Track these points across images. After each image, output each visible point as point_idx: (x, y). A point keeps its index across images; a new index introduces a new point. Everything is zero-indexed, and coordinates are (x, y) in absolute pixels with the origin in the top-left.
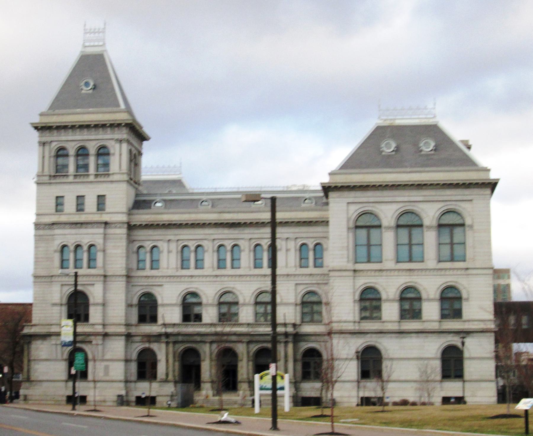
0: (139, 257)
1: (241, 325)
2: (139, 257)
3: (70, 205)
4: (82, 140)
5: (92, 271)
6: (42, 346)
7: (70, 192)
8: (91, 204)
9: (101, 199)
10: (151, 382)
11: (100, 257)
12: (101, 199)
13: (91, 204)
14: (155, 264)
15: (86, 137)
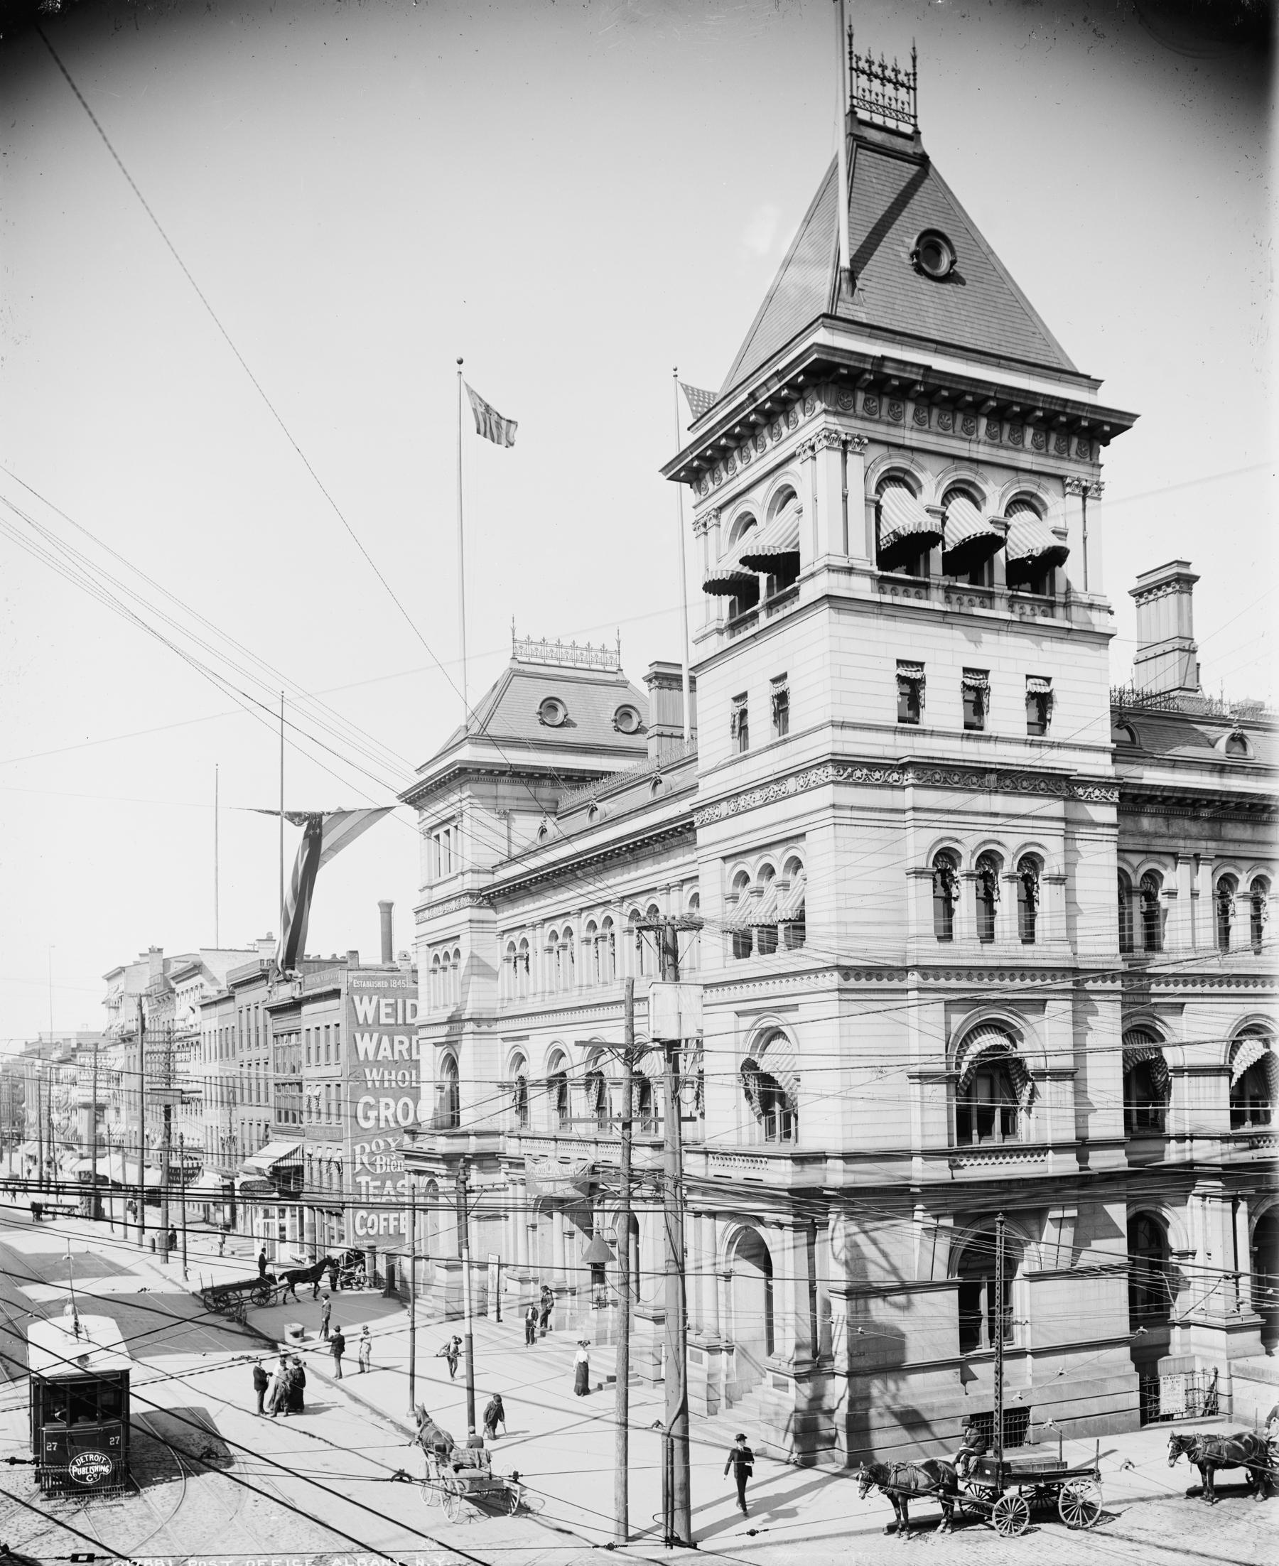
3: (943, 705)
8: (1007, 712)
13: (1007, 712)
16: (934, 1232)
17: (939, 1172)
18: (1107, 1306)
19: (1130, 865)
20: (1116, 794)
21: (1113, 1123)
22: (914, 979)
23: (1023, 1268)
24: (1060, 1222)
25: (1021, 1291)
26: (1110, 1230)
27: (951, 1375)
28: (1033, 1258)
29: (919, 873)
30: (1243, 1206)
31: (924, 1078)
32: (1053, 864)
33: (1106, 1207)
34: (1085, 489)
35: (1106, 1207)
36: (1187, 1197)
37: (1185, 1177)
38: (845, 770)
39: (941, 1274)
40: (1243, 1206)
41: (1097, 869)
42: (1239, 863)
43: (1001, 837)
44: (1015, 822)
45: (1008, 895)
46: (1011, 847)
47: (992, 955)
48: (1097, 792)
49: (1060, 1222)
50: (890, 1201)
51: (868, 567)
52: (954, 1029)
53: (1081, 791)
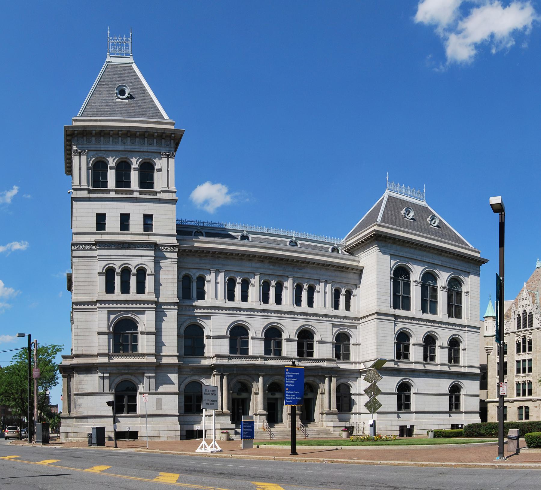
0: (190, 288)
1: (437, 365)
2: (190, 288)
3: (113, 224)
4: (124, 151)
5: (141, 297)
6: (85, 379)
7: (113, 212)
8: (136, 224)
9: (148, 218)
10: (179, 394)
11: (149, 282)
12: (148, 218)
13: (136, 224)
14: (201, 295)
15: (129, 147)
16: (103, 378)
17: (105, 360)
18: (172, 404)
20: (177, 249)
21: (79, 288)
24: (150, 377)
26: (171, 383)
28: (141, 388)
29: (99, 274)
30: (225, 378)
31: (100, 333)
33: (169, 375)
34: (168, 155)
35: (169, 375)
36: (211, 375)
39: (107, 390)
40: (225, 378)
41: (169, 274)
42: (342, 284)
43: (130, 262)
44: (143, 258)
46: (133, 265)
48: (169, 248)
49: (150, 377)
53: (163, 248)
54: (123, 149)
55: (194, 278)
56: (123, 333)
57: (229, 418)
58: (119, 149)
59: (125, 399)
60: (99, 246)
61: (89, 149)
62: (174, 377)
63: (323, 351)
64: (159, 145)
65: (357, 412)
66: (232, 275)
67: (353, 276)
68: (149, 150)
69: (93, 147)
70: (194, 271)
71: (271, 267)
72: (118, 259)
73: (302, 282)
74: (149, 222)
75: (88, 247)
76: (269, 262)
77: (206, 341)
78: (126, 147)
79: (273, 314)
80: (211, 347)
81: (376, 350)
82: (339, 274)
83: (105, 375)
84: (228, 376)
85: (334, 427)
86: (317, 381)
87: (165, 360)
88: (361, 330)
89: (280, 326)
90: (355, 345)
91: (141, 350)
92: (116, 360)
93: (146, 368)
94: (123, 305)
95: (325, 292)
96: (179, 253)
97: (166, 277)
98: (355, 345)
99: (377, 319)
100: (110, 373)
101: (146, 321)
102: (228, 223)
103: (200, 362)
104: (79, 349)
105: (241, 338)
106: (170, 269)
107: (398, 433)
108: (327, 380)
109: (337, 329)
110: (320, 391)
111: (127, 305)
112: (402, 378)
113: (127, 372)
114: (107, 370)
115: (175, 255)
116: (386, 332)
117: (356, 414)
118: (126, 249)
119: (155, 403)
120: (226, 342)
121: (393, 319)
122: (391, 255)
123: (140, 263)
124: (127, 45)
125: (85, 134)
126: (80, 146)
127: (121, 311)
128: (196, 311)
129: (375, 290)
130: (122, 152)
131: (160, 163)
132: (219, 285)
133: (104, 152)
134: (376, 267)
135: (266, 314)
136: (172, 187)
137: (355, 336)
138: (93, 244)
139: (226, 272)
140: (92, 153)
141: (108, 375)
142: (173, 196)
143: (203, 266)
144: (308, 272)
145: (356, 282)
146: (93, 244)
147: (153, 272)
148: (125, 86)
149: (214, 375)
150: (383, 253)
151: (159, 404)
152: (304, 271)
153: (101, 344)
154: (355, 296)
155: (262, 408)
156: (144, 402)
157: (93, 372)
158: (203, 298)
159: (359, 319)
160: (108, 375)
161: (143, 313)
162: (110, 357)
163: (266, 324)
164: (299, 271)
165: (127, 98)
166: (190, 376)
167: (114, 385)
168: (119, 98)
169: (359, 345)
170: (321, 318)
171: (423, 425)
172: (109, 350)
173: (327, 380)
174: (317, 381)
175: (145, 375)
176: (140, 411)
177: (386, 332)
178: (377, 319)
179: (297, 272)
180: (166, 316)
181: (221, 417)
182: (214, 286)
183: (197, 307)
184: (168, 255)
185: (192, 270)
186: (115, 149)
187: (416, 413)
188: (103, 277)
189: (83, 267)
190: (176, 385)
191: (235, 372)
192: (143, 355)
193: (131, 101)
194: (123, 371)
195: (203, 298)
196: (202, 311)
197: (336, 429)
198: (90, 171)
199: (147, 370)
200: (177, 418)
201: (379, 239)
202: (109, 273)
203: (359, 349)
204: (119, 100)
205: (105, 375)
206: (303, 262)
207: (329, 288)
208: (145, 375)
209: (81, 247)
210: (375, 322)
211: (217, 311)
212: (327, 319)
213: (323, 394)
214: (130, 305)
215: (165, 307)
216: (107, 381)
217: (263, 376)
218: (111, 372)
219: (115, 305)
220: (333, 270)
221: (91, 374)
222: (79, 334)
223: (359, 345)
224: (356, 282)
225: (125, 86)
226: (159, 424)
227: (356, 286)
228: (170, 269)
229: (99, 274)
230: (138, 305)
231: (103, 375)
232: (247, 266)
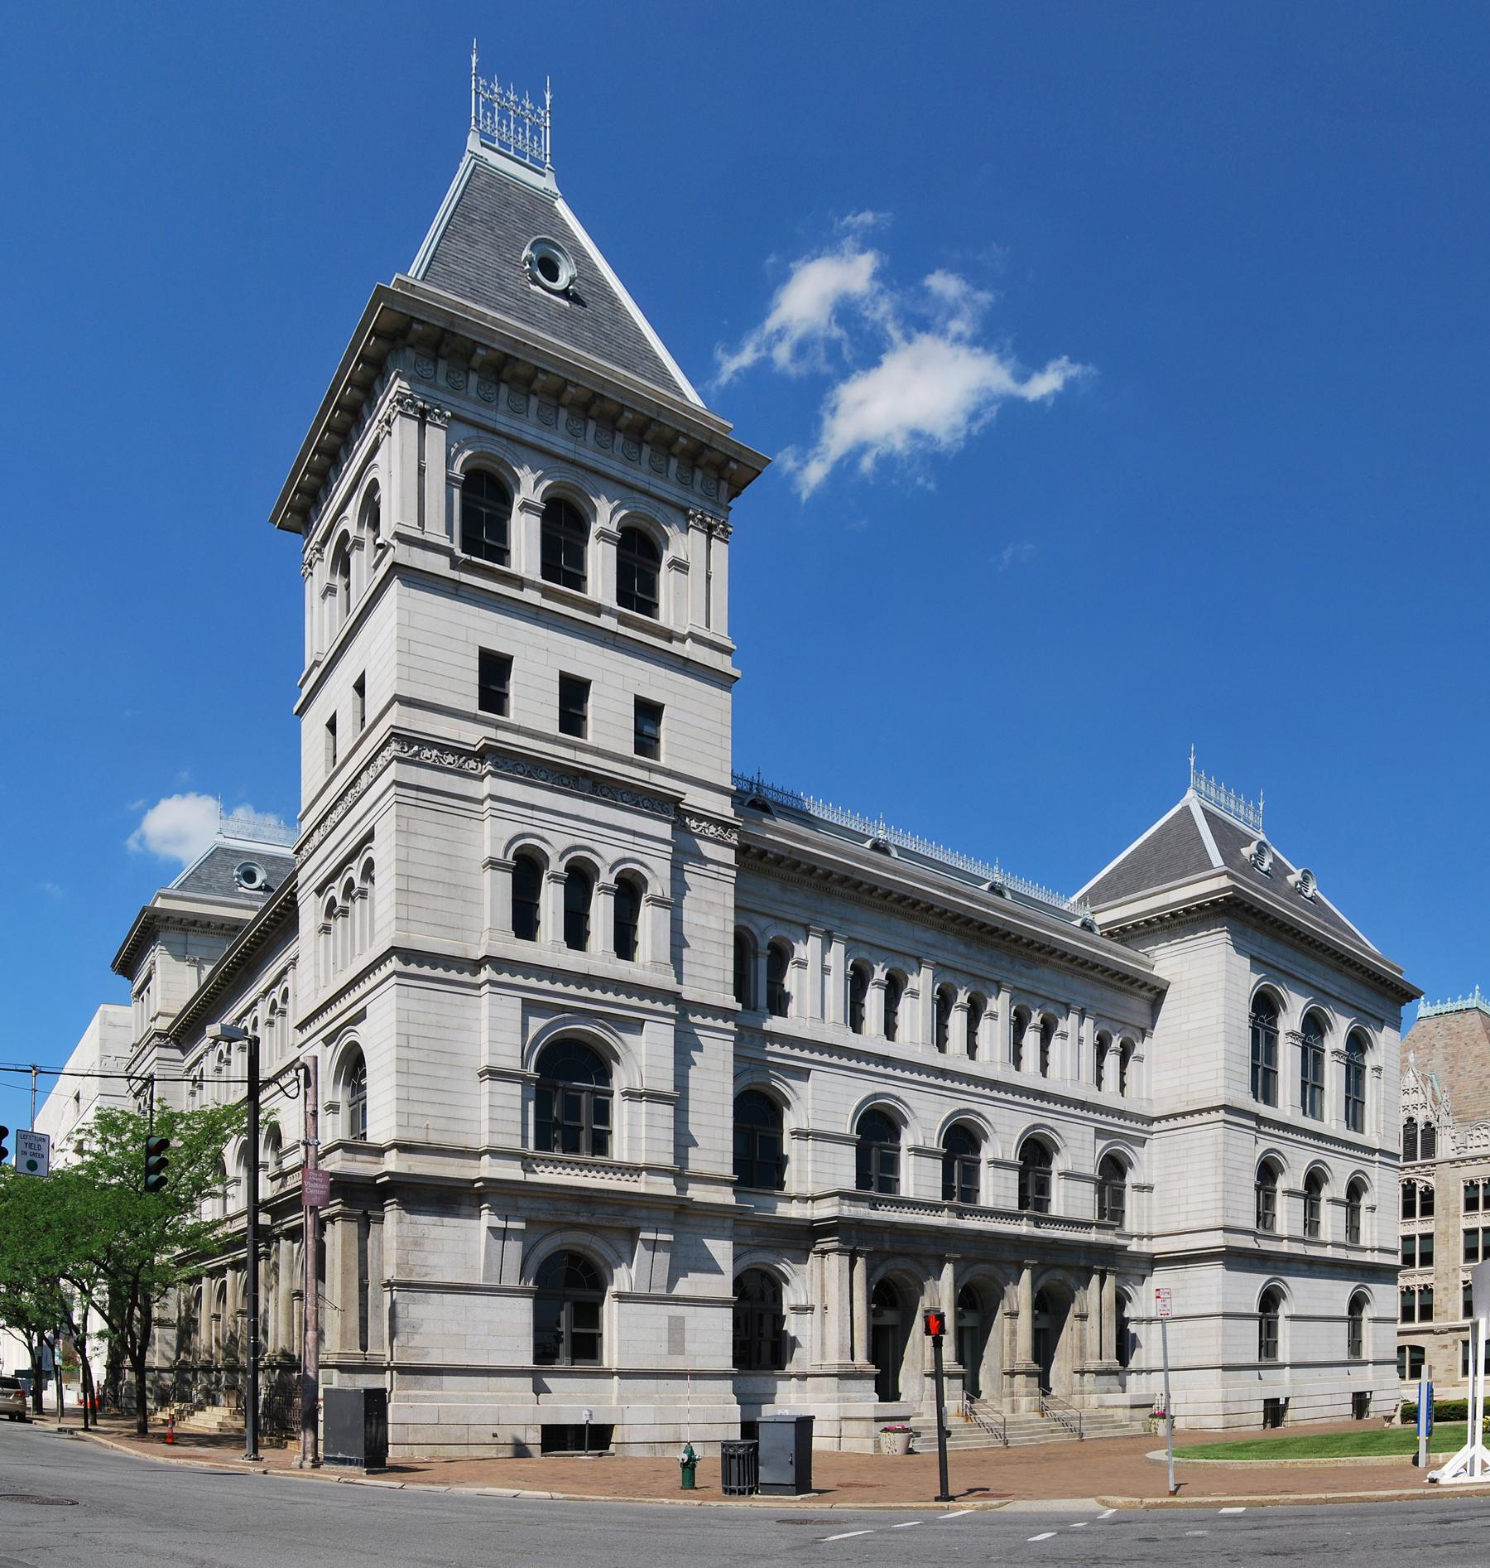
0: (760, 972)
2: (760, 972)
3: (532, 704)
4: (573, 463)
11: (650, 923)
16: (502, 1234)
17: (512, 1171)
18: (712, 1337)
19: (756, 926)
22: (486, 973)
23: (612, 1289)
25: (611, 1311)
26: (709, 1266)
27: (528, 1382)
28: (623, 1279)
29: (493, 864)
31: (494, 1074)
32: (659, 884)
33: (707, 1242)
34: (711, 528)
35: (707, 1242)
36: (808, 1251)
37: (803, 1238)
38: (410, 748)
39: (511, 1280)
41: (712, 909)
45: (601, 911)
46: (608, 857)
47: (572, 960)
48: (712, 829)
49: (654, 1246)
50: (444, 1198)
51: (445, 542)
52: (532, 1033)
53: (694, 824)
54: (571, 456)
55: (763, 945)
56: (567, 1083)
57: (871, 1384)
58: (558, 450)
59: (563, 1314)
60: (496, 766)
61: (456, 411)
62: (721, 1250)
63: (1071, 1199)
64: (684, 482)
65: (1144, 1366)
66: (864, 955)
67: (1137, 1006)
68: (653, 490)
69: (470, 411)
70: (763, 922)
71: (962, 948)
72: (565, 826)
73: (1030, 1006)
74: (648, 729)
75: (450, 759)
76: (958, 933)
77: (789, 1146)
78: (581, 450)
79: (964, 1087)
80: (810, 1167)
81: (1220, 1204)
82: (1109, 994)
83: (511, 1225)
84: (869, 1257)
85: (1132, 1407)
86: (1072, 1282)
87: (698, 1193)
88: (1155, 1150)
89: (980, 1121)
90: (1140, 1188)
91: (620, 1149)
92: (546, 1176)
93: (644, 1213)
94: (572, 989)
95: (1080, 1041)
96: (742, 851)
97: (702, 921)
98: (1140, 1188)
99: (1225, 1121)
100: (528, 1221)
101: (643, 1057)
102: (816, 799)
103: (773, 1210)
104: (415, 1121)
105: (881, 1147)
106: (712, 897)
107: (1349, 1409)
108: (1095, 1279)
109: (1105, 1143)
110: (1075, 1308)
111: (584, 992)
112: (1268, 1277)
113: (583, 1220)
114: (518, 1209)
115: (729, 856)
116: (1241, 1158)
117: (1140, 1372)
118: (584, 798)
119: (665, 1335)
120: (849, 1154)
121: (1253, 1124)
122: (1252, 958)
123: (629, 854)
124: (535, 129)
125: (444, 350)
126: (423, 389)
127: (563, 1009)
128: (769, 1048)
129: (1221, 1046)
130: (563, 465)
131: (683, 544)
132: (829, 979)
133: (504, 441)
134: (1222, 985)
135: (948, 1084)
136: (723, 638)
137: (1145, 1164)
138: (470, 755)
139: (852, 944)
140: (463, 431)
141: (521, 1225)
142: (723, 663)
143: (790, 913)
144: (1046, 979)
145: (1145, 1022)
146: (470, 755)
147: (668, 894)
148: (559, 249)
149: (824, 1252)
150: (1239, 950)
151: (676, 1335)
152: (1035, 972)
153: (498, 1114)
154: (1140, 1059)
155: (953, 1358)
156: (623, 1330)
157: (465, 1210)
158: (784, 1014)
159: (1152, 1120)
160: (521, 1225)
161: (636, 1026)
162: (527, 1163)
163: (947, 1114)
164: (1025, 971)
165: (564, 294)
166: (750, 1252)
167: (533, 1265)
168: (536, 282)
169: (1150, 1188)
170: (1072, 1111)
171: (1318, 1400)
172: (524, 1138)
173: (1095, 1279)
174: (1072, 1282)
175: (642, 1235)
176: (612, 1354)
177: (1241, 1158)
178: (1225, 1121)
179: (1020, 975)
180: (700, 1048)
181: (853, 1382)
182: (815, 980)
183: (774, 1037)
184: (708, 849)
185: (756, 917)
186: (544, 444)
187: (1293, 1366)
188: (507, 879)
189: (433, 829)
190: (728, 1278)
191: (887, 1247)
192: (634, 1170)
193: (576, 307)
194: (572, 1218)
195: (784, 1014)
196: (786, 1050)
197: (1138, 1412)
198: (457, 493)
199: (649, 1219)
200: (730, 1383)
201: (1236, 914)
202: (526, 870)
203: (1150, 1199)
204: (538, 289)
205: (511, 1225)
206: (1041, 948)
207: (1088, 1030)
208: (642, 1235)
209: (426, 753)
210: (1218, 1131)
211: (825, 1058)
212: (1084, 1113)
213: (1083, 1317)
214: (597, 994)
215: (698, 1019)
216: (514, 1248)
217: (955, 1262)
218: (534, 1215)
219: (546, 985)
220: (1100, 981)
221: (457, 1216)
222: (415, 1067)
223: (1150, 1188)
224: (1145, 1022)
225: (559, 249)
226: (676, 1401)
227: (1143, 1033)
228: (712, 897)
229: (493, 864)
230: (622, 999)
231: (502, 1224)
232: (906, 934)
